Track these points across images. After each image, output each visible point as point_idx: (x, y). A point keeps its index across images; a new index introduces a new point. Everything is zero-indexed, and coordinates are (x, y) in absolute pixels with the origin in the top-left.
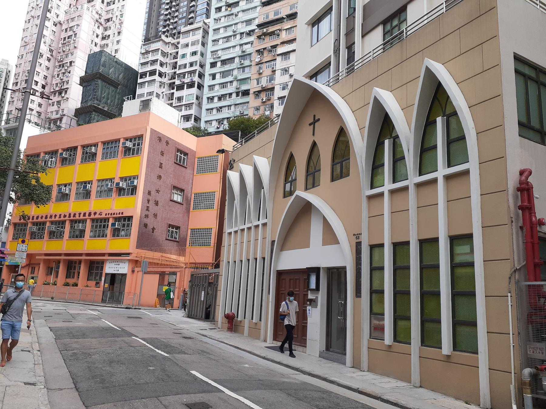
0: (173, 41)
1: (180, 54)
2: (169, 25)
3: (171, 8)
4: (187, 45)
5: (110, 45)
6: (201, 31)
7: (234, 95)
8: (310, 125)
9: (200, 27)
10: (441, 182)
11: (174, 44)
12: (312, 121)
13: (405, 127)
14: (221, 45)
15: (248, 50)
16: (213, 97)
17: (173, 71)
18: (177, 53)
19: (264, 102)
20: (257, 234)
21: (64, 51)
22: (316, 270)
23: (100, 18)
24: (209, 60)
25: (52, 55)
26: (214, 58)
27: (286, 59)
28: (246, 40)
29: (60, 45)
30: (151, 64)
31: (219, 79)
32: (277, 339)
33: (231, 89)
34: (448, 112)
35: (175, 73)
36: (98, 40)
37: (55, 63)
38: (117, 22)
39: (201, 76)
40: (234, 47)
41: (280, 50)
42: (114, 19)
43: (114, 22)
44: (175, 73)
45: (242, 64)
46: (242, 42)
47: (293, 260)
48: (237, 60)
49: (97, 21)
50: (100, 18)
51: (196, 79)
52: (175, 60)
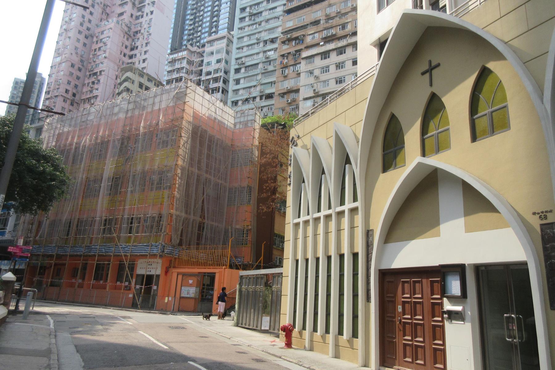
0: (199, 50)
1: (205, 62)
2: (192, 39)
3: (194, 23)
4: (212, 53)
5: (138, 55)
6: (225, 41)
7: (258, 99)
8: (423, 74)
9: (225, 37)
11: (199, 53)
12: (426, 67)
13: (329, 160)
14: (246, 52)
15: (271, 57)
16: (238, 101)
17: (198, 78)
18: (202, 61)
19: (290, 103)
20: (339, 224)
21: (94, 62)
22: (459, 269)
23: (129, 31)
24: (233, 66)
25: (83, 66)
26: (238, 64)
27: (310, 63)
28: (270, 46)
29: (91, 56)
30: (177, 72)
31: (243, 84)
32: (386, 364)
33: (255, 92)
35: (200, 80)
36: (127, 52)
37: (86, 73)
38: (146, 34)
39: (225, 82)
40: (258, 53)
41: (305, 54)
42: (142, 31)
43: (142, 34)
44: (200, 80)
45: (266, 69)
46: (266, 49)
47: (412, 254)
48: (260, 66)
49: (126, 33)
50: (129, 31)
51: (220, 84)
52: (200, 68)
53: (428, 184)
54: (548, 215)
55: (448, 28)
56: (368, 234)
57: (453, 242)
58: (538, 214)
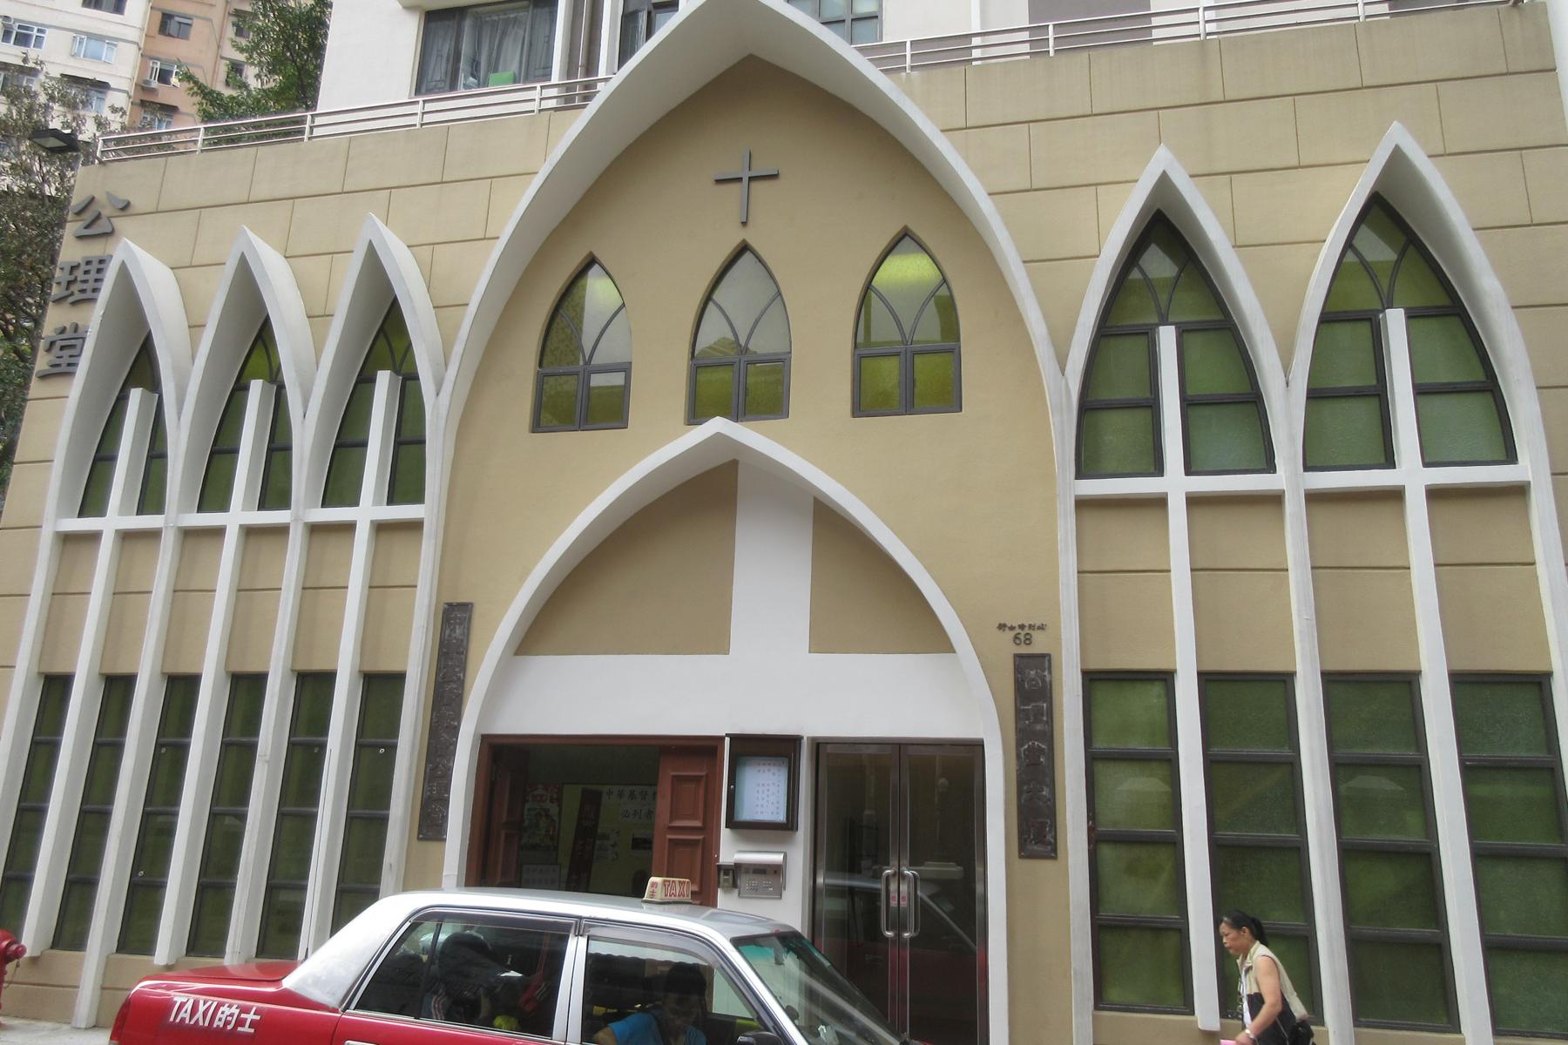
10: (362, 535)
13: (311, 360)
34: (405, 369)
53: (703, 500)
54: (1036, 635)
55: (798, 77)
56: (455, 623)
57: (765, 669)
58: (1012, 628)
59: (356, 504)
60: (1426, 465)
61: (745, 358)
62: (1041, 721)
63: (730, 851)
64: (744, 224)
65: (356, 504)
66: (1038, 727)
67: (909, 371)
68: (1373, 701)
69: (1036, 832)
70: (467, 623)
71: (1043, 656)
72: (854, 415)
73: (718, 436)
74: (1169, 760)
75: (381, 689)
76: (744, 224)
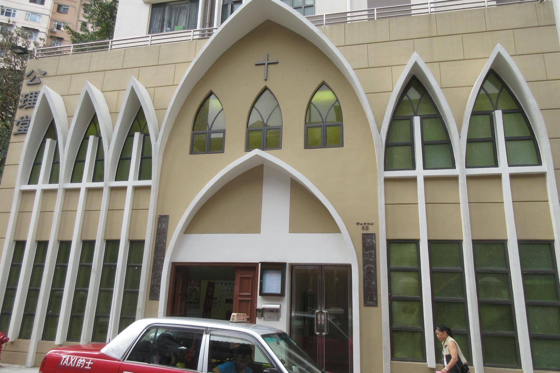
10: (129, 191)
13: (111, 129)
34: (144, 132)
53: (251, 178)
54: (370, 227)
55: (285, 27)
56: (162, 222)
57: (273, 239)
58: (361, 224)
59: (127, 180)
60: (509, 166)
61: (266, 128)
62: (372, 257)
63: (261, 304)
64: (266, 80)
65: (127, 180)
66: (371, 260)
67: (325, 132)
68: (490, 250)
69: (370, 297)
70: (167, 222)
71: (372, 234)
72: (305, 148)
73: (257, 155)
74: (418, 271)
75: (136, 246)
76: (266, 80)
